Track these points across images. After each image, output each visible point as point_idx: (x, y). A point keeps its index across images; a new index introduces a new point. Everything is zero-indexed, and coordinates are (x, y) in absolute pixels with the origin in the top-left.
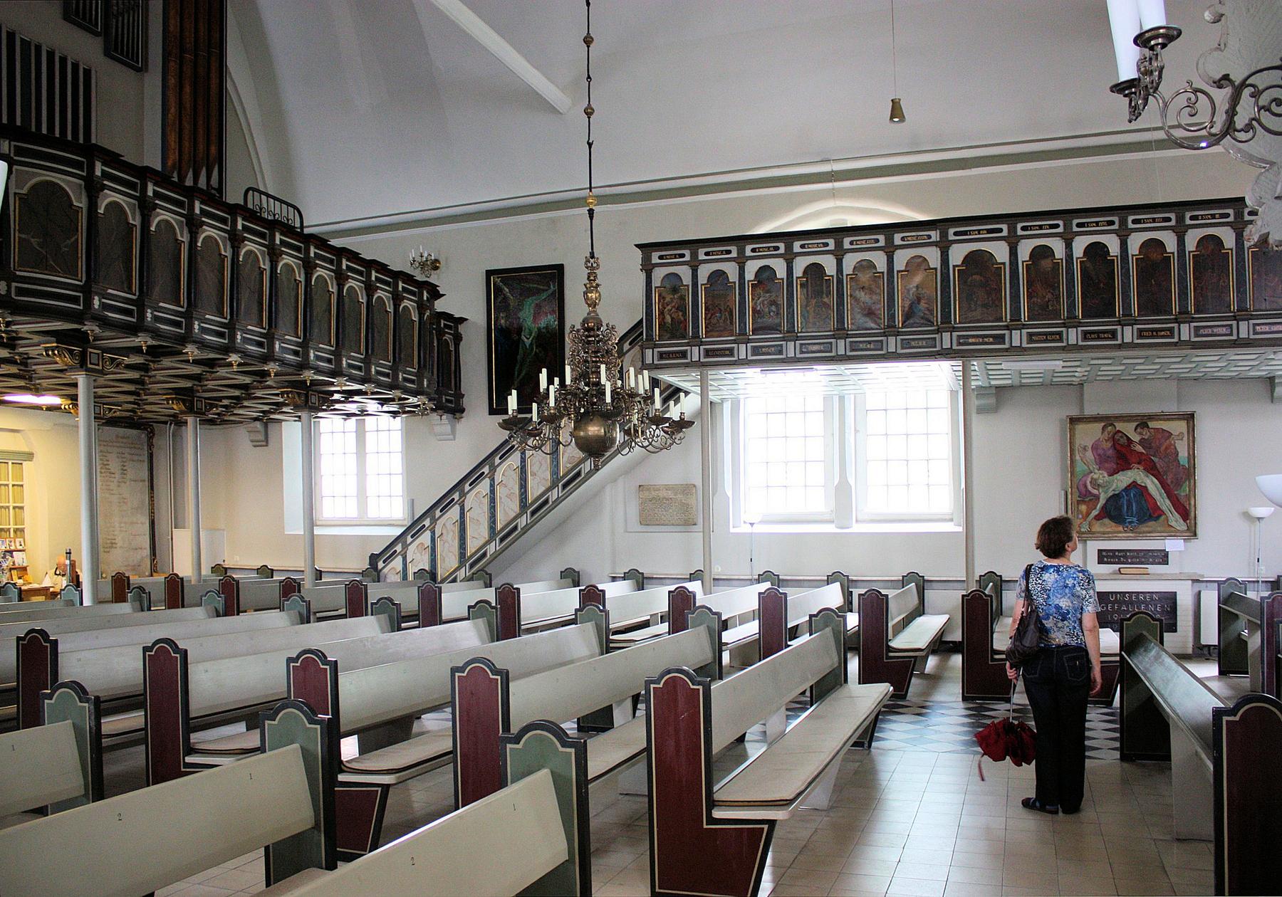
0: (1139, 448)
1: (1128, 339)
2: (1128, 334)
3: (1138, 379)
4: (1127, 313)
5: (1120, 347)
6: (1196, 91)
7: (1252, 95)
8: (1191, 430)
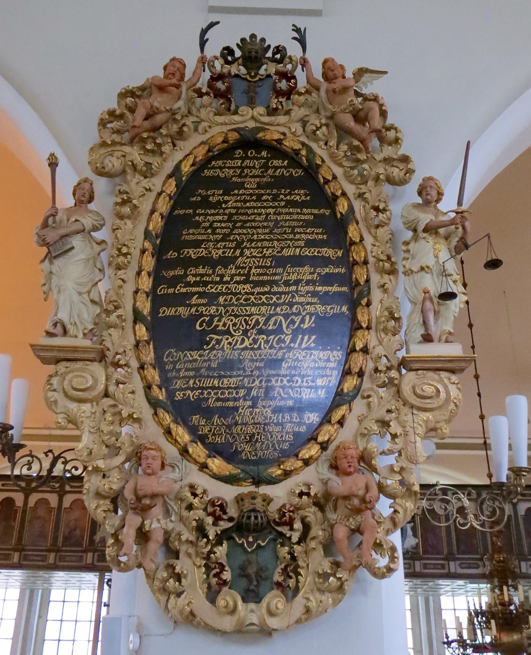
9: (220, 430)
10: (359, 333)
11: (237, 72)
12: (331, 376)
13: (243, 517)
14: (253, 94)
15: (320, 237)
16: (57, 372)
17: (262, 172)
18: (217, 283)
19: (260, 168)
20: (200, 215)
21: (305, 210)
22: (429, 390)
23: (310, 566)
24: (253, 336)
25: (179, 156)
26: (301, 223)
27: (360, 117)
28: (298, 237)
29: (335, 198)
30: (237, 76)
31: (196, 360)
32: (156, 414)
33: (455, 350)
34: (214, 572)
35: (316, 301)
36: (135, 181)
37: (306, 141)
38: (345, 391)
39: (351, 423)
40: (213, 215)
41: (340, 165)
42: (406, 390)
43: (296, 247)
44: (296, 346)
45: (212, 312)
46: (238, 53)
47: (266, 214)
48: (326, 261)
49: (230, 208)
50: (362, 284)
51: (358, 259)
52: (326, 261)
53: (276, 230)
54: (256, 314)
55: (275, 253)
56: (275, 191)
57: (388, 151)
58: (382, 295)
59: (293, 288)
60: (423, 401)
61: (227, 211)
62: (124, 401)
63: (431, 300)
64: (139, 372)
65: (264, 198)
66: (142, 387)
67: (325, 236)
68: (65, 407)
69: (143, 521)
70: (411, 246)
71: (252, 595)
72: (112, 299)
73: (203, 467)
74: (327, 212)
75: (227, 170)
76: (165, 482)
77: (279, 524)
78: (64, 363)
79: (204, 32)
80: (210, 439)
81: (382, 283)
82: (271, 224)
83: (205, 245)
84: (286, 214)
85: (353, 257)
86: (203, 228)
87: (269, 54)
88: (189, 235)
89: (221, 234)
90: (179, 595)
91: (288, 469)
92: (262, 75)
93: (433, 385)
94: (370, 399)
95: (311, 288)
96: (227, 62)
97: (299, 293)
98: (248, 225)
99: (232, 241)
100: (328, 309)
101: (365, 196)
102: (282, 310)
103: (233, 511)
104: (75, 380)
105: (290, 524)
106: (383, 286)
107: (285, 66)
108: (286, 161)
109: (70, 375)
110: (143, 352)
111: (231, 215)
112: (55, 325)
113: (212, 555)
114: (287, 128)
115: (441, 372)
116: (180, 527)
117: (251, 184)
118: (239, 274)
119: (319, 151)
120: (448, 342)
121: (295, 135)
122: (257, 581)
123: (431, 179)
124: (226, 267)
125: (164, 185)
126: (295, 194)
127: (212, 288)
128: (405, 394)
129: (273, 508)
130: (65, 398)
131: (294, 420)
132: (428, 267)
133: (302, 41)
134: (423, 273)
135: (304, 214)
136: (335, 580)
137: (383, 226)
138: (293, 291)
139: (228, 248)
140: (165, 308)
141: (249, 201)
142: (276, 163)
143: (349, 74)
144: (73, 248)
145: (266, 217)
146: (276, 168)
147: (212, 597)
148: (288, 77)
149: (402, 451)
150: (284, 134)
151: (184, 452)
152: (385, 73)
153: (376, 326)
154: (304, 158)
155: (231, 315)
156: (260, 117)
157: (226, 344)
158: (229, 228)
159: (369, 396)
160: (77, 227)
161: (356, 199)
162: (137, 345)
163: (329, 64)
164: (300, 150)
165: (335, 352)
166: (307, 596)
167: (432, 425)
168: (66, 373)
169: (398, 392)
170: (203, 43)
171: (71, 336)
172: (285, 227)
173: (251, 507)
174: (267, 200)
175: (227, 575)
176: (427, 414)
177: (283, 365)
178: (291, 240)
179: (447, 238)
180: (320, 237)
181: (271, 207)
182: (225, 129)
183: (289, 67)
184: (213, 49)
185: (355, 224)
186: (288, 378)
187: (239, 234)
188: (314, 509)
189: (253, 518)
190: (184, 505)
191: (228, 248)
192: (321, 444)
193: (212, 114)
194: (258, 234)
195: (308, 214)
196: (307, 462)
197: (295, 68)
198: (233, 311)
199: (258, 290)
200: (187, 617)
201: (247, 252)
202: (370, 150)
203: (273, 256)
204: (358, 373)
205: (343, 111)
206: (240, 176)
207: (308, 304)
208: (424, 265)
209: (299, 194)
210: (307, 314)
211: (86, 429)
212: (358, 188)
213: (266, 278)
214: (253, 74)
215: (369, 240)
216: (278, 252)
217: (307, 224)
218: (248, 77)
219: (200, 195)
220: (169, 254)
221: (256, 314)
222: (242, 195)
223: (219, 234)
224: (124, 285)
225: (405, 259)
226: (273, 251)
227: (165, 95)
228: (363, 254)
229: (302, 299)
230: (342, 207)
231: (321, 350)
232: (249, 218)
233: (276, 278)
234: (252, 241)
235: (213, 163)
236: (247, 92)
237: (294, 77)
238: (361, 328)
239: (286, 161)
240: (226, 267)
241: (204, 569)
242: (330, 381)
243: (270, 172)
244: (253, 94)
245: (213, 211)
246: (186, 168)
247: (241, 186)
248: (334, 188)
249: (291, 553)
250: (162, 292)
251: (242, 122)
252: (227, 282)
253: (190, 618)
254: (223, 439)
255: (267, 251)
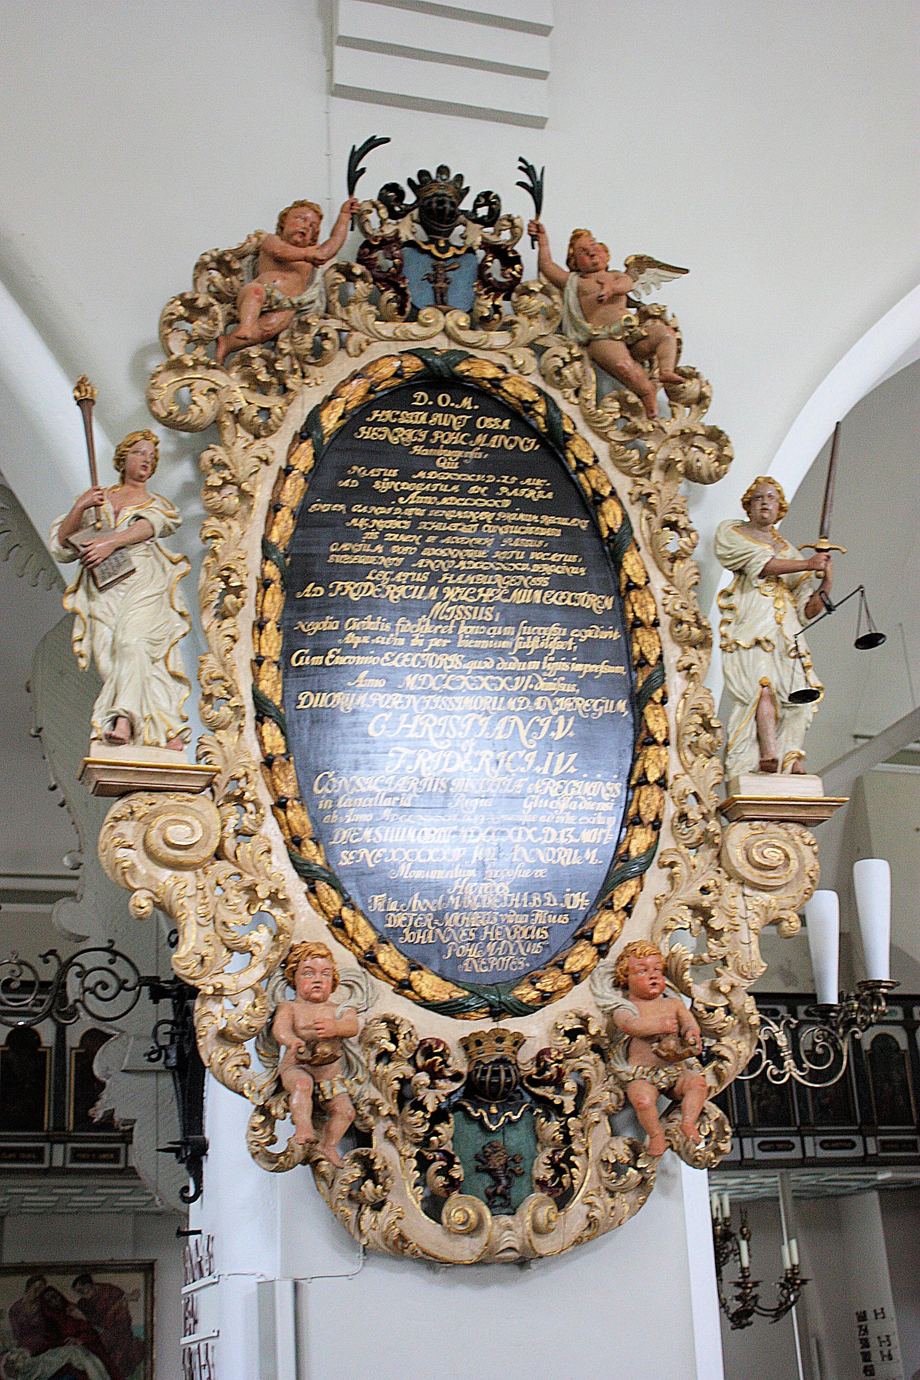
0: (78, 1314)
1: (58, 1162)
2: (58, 1155)
3: (78, 1212)
4: (59, 1124)
5: (46, 1173)
6: (21, 963)
7: (78, 975)
8: (150, 1285)
9: (423, 921)
10: (651, 751)
11: (411, 238)
12: (604, 826)
13: (477, 1071)
14: (444, 285)
15: (574, 570)
16: (132, 813)
17: (465, 439)
18: (399, 649)
19: (463, 430)
20: (359, 516)
21: (546, 519)
22: (773, 856)
23: (590, 1151)
24: (471, 751)
25: (311, 397)
26: (541, 542)
27: (643, 350)
28: (536, 568)
29: (598, 499)
30: (411, 244)
31: (373, 794)
32: (313, 890)
33: (809, 788)
34: (437, 1165)
35: (573, 690)
36: (241, 444)
37: (541, 384)
38: (634, 853)
39: (644, 910)
40: (384, 517)
41: (604, 437)
42: (736, 855)
43: (535, 588)
44: (545, 771)
45: (395, 703)
46: (410, 198)
47: (479, 521)
48: (586, 617)
49: (414, 506)
50: (652, 662)
51: (644, 617)
52: (586, 617)
53: (497, 554)
54: (473, 711)
55: (499, 597)
56: (491, 479)
57: (685, 418)
58: (686, 683)
59: (534, 665)
60: (763, 873)
61: (409, 512)
62: (254, 866)
63: (772, 698)
64: (275, 815)
65: (473, 490)
66: (281, 842)
67: (582, 570)
68: (150, 877)
69: (317, 1084)
70: (735, 600)
71: (502, 1201)
72: (214, 675)
73: (403, 986)
74: (584, 524)
75: (402, 429)
76: (338, 1012)
77: (537, 1084)
78: (144, 795)
79: (356, 156)
80: (408, 938)
81: (686, 662)
82: (489, 542)
83: (374, 575)
84: (514, 523)
85: (633, 611)
86: (367, 541)
87: (467, 204)
88: (342, 554)
89: (401, 556)
90: (378, 1206)
91: (549, 989)
92: (459, 248)
93: (778, 848)
94: (676, 869)
95: (564, 666)
96: (393, 215)
97: (544, 674)
98: (448, 540)
99: (423, 570)
100: (595, 705)
101: (651, 500)
102: (517, 705)
103: (458, 1062)
104: (170, 828)
105: (558, 1083)
106: (688, 668)
107: (498, 233)
108: (508, 421)
109: (161, 819)
110: (282, 776)
111: (416, 520)
112: (114, 722)
113: (434, 1138)
114: (503, 356)
115: (790, 825)
116: (371, 1093)
117: (448, 460)
118: (438, 635)
119: (563, 406)
120: (798, 773)
121: (521, 372)
122: (507, 1177)
123: (770, 481)
124: (414, 620)
125: (290, 454)
126: (525, 486)
127: (392, 659)
128: (734, 862)
129: (526, 1056)
130: (149, 863)
131: (548, 904)
132: (767, 641)
133: (536, 192)
134: (758, 650)
135: (543, 526)
136: (635, 1172)
137: (682, 558)
138: (534, 671)
139: (416, 583)
140: (309, 693)
141: (448, 495)
142: (491, 423)
143: (616, 264)
144: (133, 571)
145: (479, 528)
146: (491, 433)
147: (434, 1207)
148: (509, 259)
149: (728, 958)
150: (502, 368)
151: (369, 960)
152: (686, 271)
153: (678, 741)
154: (541, 420)
155: (428, 711)
156: (459, 332)
157: (424, 764)
158: (413, 544)
159: (672, 865)
160: (141, 529)
161: (632, 503)
162: (268, 762)
163: (583, 242)
164: (535, 402)
165: (609, 784)
166: (589, 1200)
167: (774, 915)
168: (155, 814)
169: (718, 856)
170: (354, 176)
171: (145, 744)
172: (514, 548)
173: (498, 1055)
174: (478, 496)
175: (457, 1172)
176: (767, 896)
177: (525, 805)
178: (525, 574)
179: (792, 589)
180: (574, 570)
181: (486, 509)
182: (396, 348)
183: (506, 235)
184: (368, 190)
185: (635, 551)
186: (535, 829)
187: (433, 558)
188: (593, 1056)
189: (503, 1074)
190: (374, 1053)
191: (416, 583)
192: (598, 945)
193: (371, 318)
194: (467, 559)
195: (552, 526)
196: (576, 978)
197: (515, 237)
198: (432, 704)
199: (472, 666)
200: (395, 1243)
201: (450, 593)
202: (656, 413)
203: (496, 603)
204: (652, 823)
205: (611, 337)
206: (426, 444)
207: (561, 694)
208: (761, 638)
209: (533, 487)
210: (560, 713)
211: (192, 918)
212: (635, 484)
213: (485, 644)
214: (442, 244)
215: (658, 583)
216: (504, 596)
217: (550, 546)
218: (432, 248)
219: (355, 476)
220: (308, 590)
221: (473, 711)
222: (433, 481)
223: (395, 555)
224: (235, 646)
225: (725, 622)
226: (496, 594)
227: (291, 276)
228: (651, 609)
229: (550, 686)
230: (611, 517)
231: (586, 779)
232: (449, 528)
233: (505, 644)
234: (458, 572)
235: (376, 414)
236: (432, 279)
237: (517, 260)
238: (655, 742)
239: (508, 421)
240: (414, 620)
241: (414, 1163)
242: (604, 835)
243: (480, 439)
244: (444, 285)
245: (383, 510)
246: (330, 421)
247: (429, 463)
248: (597, 483)
249: (565, 1129)
250: (300, 663)
251: (424, 338)
252: (418, 649)
253: (399, 1248)
254: (430, 937)
255: (485, 592)
